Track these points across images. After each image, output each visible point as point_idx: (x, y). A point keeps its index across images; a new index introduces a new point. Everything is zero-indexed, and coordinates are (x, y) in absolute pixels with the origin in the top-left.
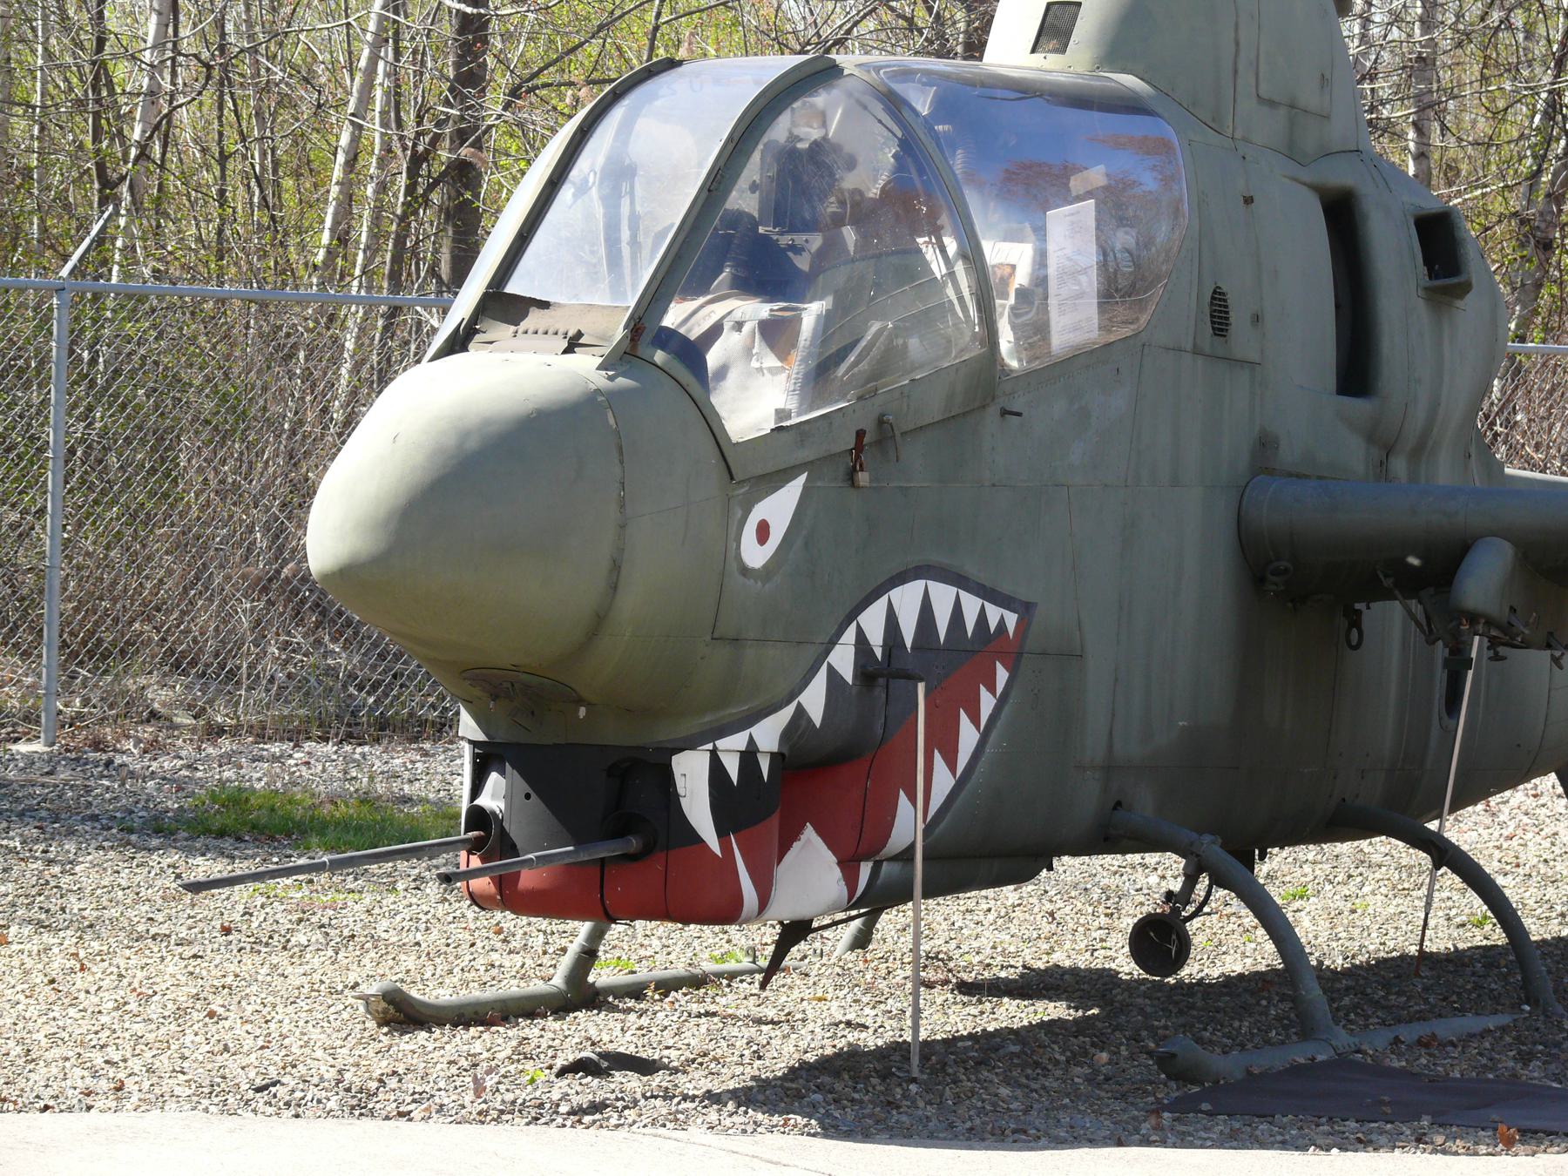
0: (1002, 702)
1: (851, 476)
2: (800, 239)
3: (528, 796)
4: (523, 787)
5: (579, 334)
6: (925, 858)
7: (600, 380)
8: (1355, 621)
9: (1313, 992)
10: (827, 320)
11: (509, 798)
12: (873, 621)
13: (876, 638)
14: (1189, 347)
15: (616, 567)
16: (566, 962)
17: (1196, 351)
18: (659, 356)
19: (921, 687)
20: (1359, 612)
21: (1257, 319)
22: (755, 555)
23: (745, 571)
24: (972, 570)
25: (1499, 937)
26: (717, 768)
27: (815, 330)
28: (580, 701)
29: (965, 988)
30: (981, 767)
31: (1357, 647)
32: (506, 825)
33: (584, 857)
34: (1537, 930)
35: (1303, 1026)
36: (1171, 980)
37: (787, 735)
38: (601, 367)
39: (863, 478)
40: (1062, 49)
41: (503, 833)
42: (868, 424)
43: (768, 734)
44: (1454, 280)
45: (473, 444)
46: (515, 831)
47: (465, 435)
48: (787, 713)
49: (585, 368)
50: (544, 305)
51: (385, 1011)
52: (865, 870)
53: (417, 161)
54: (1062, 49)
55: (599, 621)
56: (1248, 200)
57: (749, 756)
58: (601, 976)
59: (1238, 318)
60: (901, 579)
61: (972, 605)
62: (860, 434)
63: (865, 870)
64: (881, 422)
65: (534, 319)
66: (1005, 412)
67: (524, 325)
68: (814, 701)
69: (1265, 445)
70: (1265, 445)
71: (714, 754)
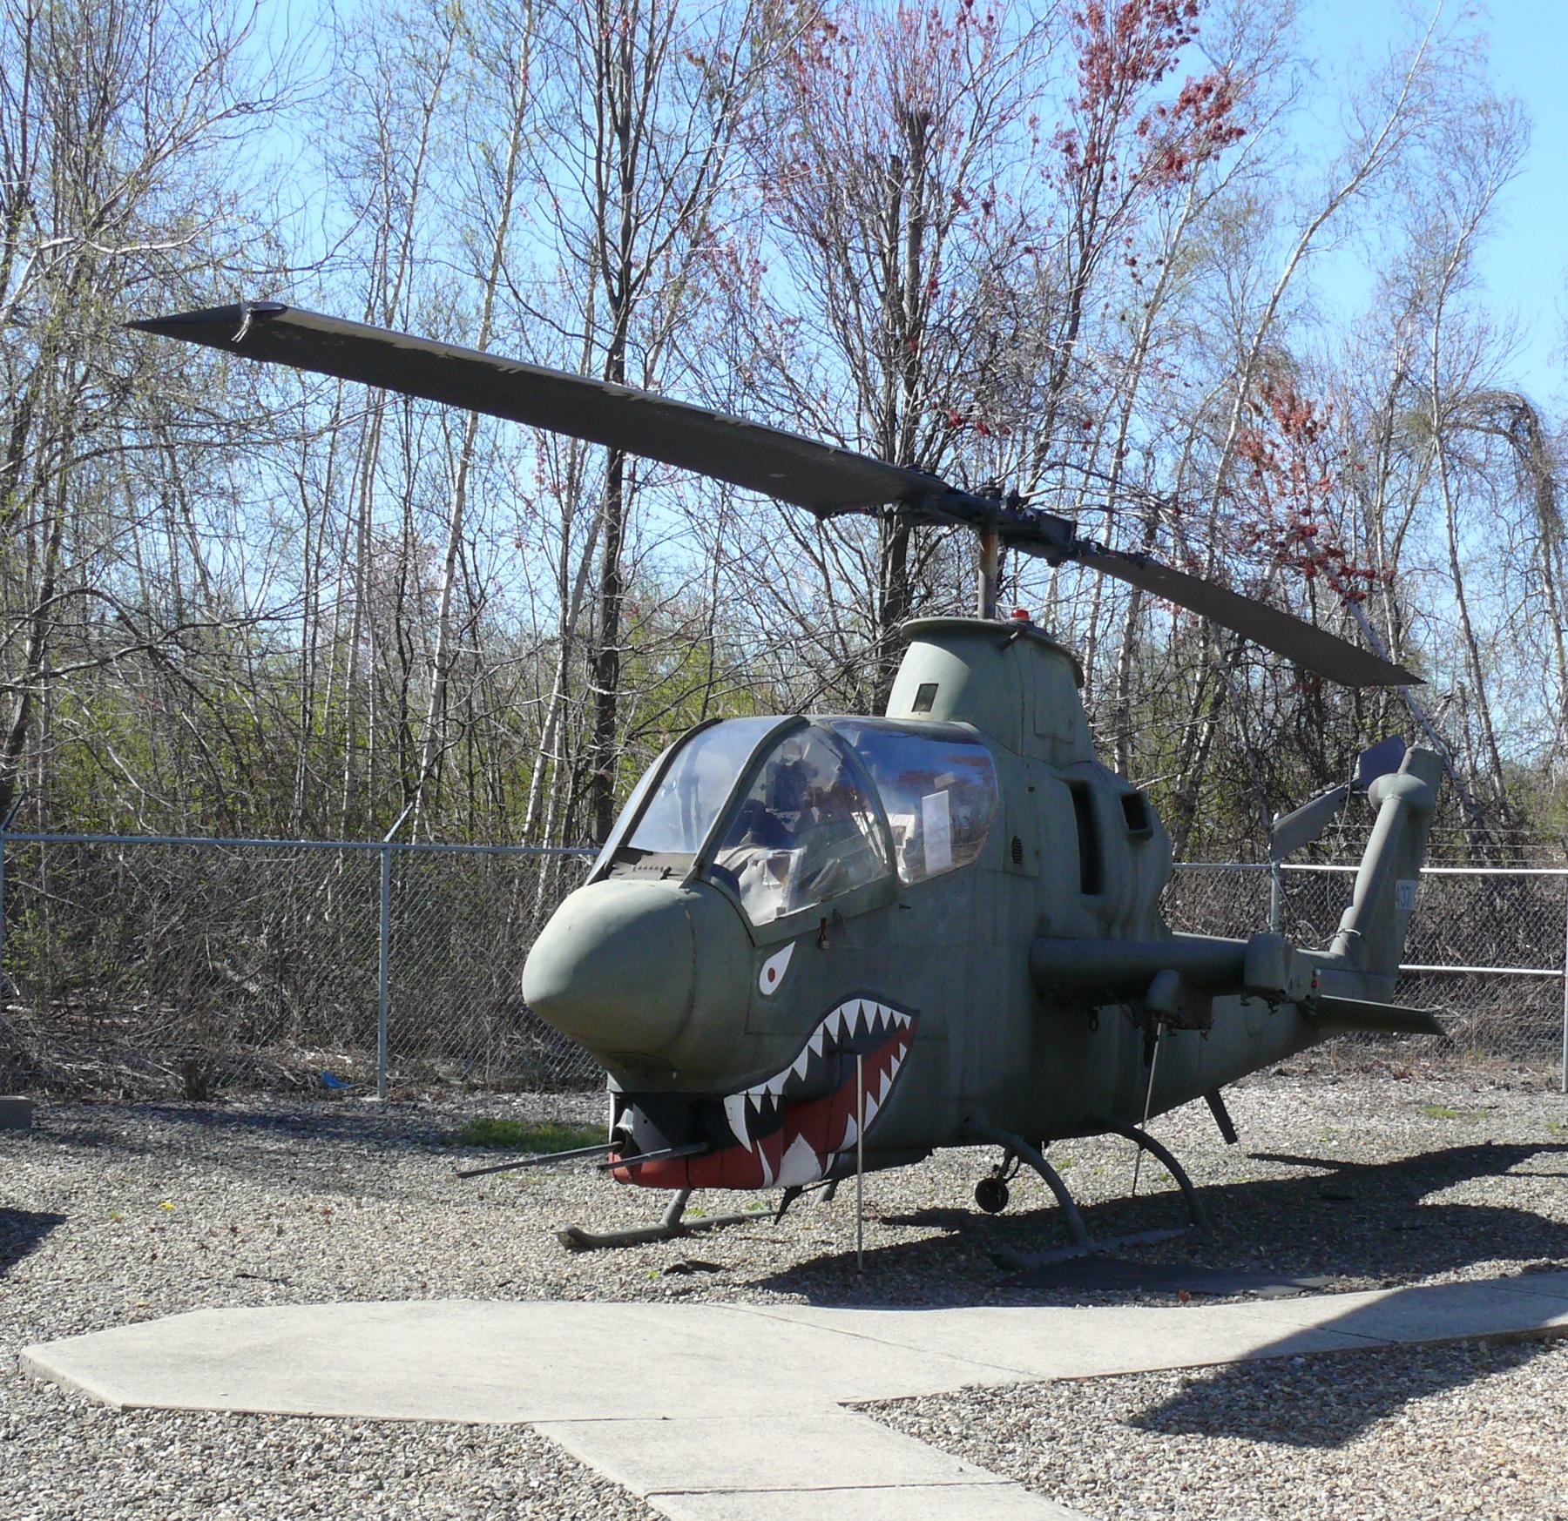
1: (819, 942)
4: (642, 1116)
7: (681, 893)
9: (1076, 1219)
10: (804, 859)
11: (635, 1123)
12: (832, 1022)
17: (1005, 871)
18: (713, 880)
21: (1037, 853)
22: (768, 987)
23: (762, 995)
26: (749, 1105)
28: (673, 1070)
30: (893, 1100)
34: (1196, 1182)
39: (826, 944)
41: (633, 1142)
43: (776, 1085)
45: (612, 929)
47: (608, 925)
48: (787, 1073)
50: (651, 853)
52: (831, 1158)
55: (684, 1024)
57: (766, 1097)
58: (686, 1219)
61: (886, 1012)
62: (823, 920)
63: (831, 1158)
64: (834, 914)
66: (902, 907)
68: (801, 1065)
71: (747, 1096)
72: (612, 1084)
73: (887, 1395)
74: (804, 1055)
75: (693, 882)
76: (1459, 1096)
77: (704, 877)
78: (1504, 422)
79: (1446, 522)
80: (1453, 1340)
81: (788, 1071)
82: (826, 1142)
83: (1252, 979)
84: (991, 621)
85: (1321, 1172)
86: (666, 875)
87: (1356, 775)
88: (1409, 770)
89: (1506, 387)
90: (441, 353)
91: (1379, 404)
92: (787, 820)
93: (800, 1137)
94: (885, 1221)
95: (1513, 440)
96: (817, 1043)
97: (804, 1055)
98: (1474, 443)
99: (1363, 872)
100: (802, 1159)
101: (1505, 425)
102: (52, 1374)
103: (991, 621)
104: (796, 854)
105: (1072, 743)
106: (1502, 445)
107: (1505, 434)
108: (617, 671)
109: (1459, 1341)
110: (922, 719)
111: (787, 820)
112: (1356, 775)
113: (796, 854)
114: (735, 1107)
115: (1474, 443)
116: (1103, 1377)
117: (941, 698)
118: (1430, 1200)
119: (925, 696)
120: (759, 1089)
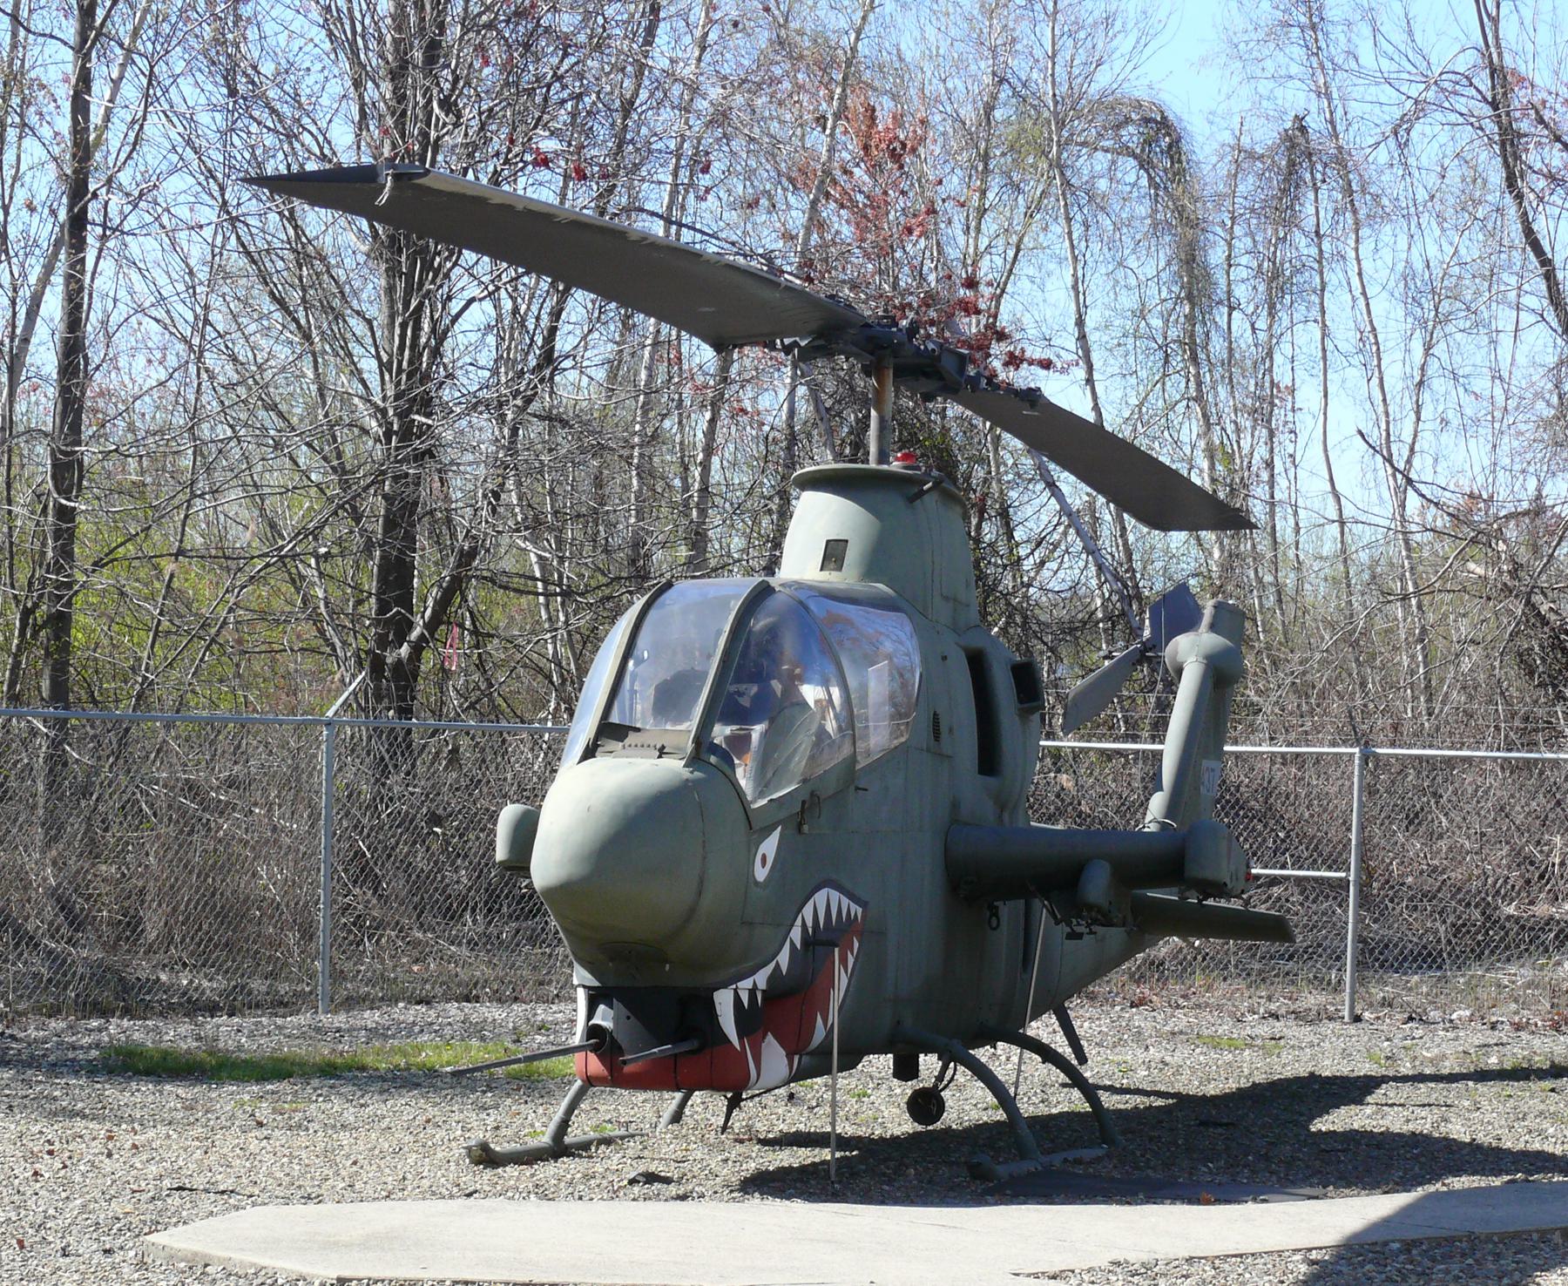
0: (856, 959)
1: (800, 825)
2: (743, 687)
3: (628, 1018)
4: (624, 1011)
5: (663, 747)
6: (832, 1053)
7: (686, 773)
8: (995, 913)
9: (1025, 1131)
10: (765, 735)
11: (616, 1020)
12: (808, 911)
13: (809, 923)
14: (925, 747)
15: (701, 882)
16: (552, 1126)
17: (928, 750)
18: (713, 759)
19: (837, 950)
20: (997, 907)
21: (951, 730)
22: (761, 874)
23: (756, 883)
24: (848, 885)
25: (1000, 1115)
26: (737, 999)
27: (760, 742)
28: (666, 961)
29: (764, 1142)
30: (847, 1001)
31: (995, 929)
32: (614, 1035)
33: (676, 1051)
34: (1027, 1108)
35: (1023, 1154)
36: (930, 1128)
37: (770, 979)
38: (685, 766)
39: (806, 828)
40: (840, 568)
41: (613, 1039)
42: (806, 797)
43: (761, 979)
44: (1035, 704)
45: (632, 811)
46: (621, 1039)
47: (627, 806)
48: (772, 966)
49: (674, 768)
50: (638, 730)
51: (480, 1156)
52: (796, 1058)
53: (27, 613)
54: (840, 568)
55: (692, 911)
56: (944, 658)
57: (752, 992)
58: (573, 1136)
59: (944, 729)
60: (818, 889)
61: (845, 901)
62: (804, 802)
63: (796, 1058)
64: (812, 794)
65: (632, 738)
66: (857, 788)
67: (627, 741)
68: (784, 958)
69: (955, 805)
70: (955, 805)
71: (736, 990)
72: (581, 976)
73: (1056, 1269)
74: (787, 948)
75: (695, 760)
76: (1208, 1023)
77: (703, 756)
78: (1131, 134)
79: (1069, 281)
80: (1524, 1232)
81: (773, 965)
82: (795, 1044)
83: (1193, 871)
84: (885, 467)
85: (1160, 1102)
86: (662, 752)
87: (1147, 633)
88: (1213, 627)
89: (1141, 93)
90: (520, 207)
91: (969, 113)
92: (741, 694)
93: (770, 1037)
94: (764, 1142)
95: (1145, 164)
96: (796, 934)
97: (787, 948)
98: (1092, 166)
99: (1171, 748)
100: (775, 1059)
101: (1134, 143)
102: (211, 1257)
103: (885, 467)
104: (757, 731)
105: (968, 606)
106: (1129, 170)
107: (1135, 156)
108: (81, 478)
109: (1529, 1232)
110: (831, 578)
111: (741, 694)
112: (1147, 633)
113: (757, 731)
114: (724, 1002)
115: (1092, 166)
116: (1228, 1256)
117: (852, 555)
118: (1321, 1125)
119: (834, 553)
120: (746, 984)
